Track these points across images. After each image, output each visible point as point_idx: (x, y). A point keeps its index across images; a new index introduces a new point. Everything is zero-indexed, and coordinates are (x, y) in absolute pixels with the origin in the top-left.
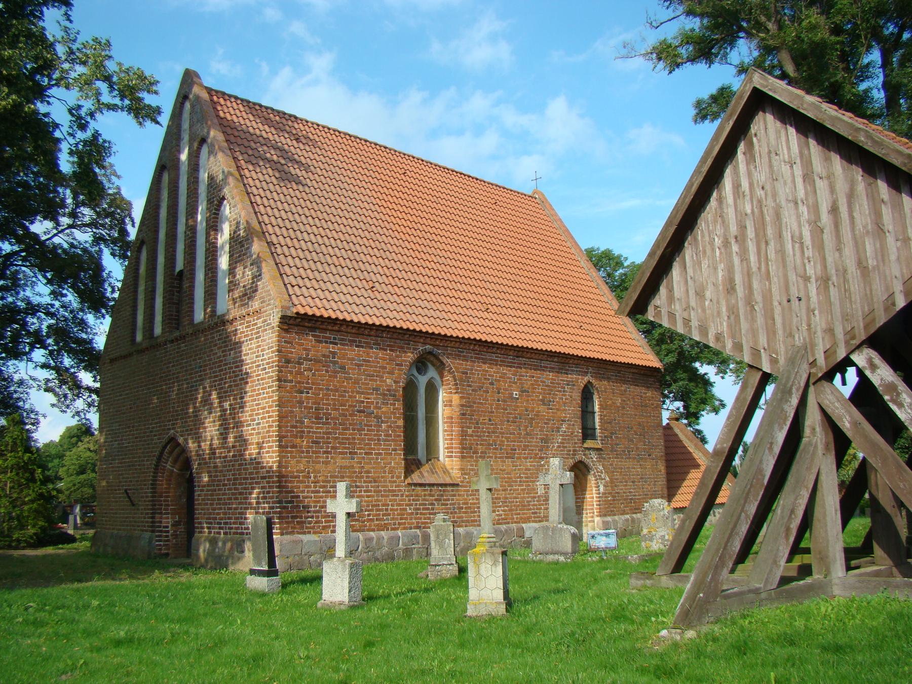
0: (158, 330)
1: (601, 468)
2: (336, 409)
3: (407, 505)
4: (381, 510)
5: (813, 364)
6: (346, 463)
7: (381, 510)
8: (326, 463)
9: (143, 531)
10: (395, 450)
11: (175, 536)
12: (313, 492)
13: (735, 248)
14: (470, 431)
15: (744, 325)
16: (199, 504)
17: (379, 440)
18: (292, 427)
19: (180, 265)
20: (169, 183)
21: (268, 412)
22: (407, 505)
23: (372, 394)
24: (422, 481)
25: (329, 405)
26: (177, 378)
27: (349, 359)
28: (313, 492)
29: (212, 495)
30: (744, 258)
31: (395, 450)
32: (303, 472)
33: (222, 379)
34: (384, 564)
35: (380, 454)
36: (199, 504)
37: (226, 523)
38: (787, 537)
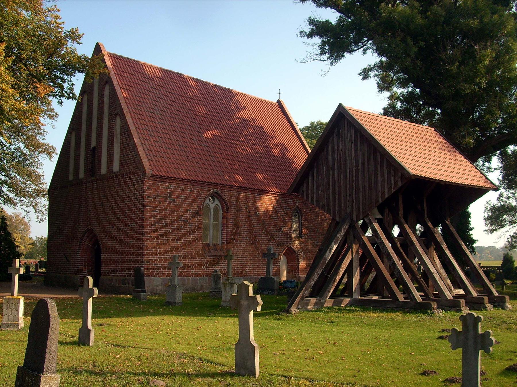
0: (81, 175)
2: (170, 220)
3: (202, 265)
4: (190, 267)
7: (190, 267)
8: (165, 244)
9: (73, 274)
12: (159, 258)
13: (331, 172)
16: (103, 262)
17: (190, 234)
18: (150, 227)
19: (93, 144)
20: (88, 101)
21: (139, 220)
22: (202, 265)
23: (187, 212)
24: (210, 254)
25: (167, 217)
26: (92, 200)
27: (177, 196)
28: (159, 258)
29: (110, 258)
32: (154, 248)
33: (116, 203)
35: (191, 241)
36: (103, 262)
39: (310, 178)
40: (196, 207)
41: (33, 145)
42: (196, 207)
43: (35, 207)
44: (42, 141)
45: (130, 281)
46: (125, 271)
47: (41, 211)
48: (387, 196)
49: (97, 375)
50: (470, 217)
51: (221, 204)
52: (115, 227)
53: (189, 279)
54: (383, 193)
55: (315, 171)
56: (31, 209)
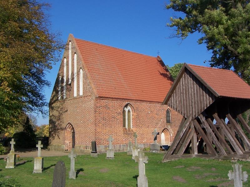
1: (171, 130)
5: (193, 117)
6: (110, 129)
10: (120, 126)
11: (69, 145)
13: (182, 95)
14: (138, 122)
15: (183, 109)
30: (183, 97)
31: (120, 126)
34: (226, 17)
37: (83, 143)
38: (185, 147)
39: (172, 98)
40: (119, 111)
41: (40, 81)
42: (119, 111)
43: (42, 112)
44: (44, 79)
45: (89, 147)
46: (87, 143)
47: (44, 113)
48: (208, 106)
49: (78, 176)
50: (24, 152)
51: (132, 109)
52: (82, 122)
53: (117, 146)
54: (207, 105)
55: (175, 94)
56: (40, 113)
